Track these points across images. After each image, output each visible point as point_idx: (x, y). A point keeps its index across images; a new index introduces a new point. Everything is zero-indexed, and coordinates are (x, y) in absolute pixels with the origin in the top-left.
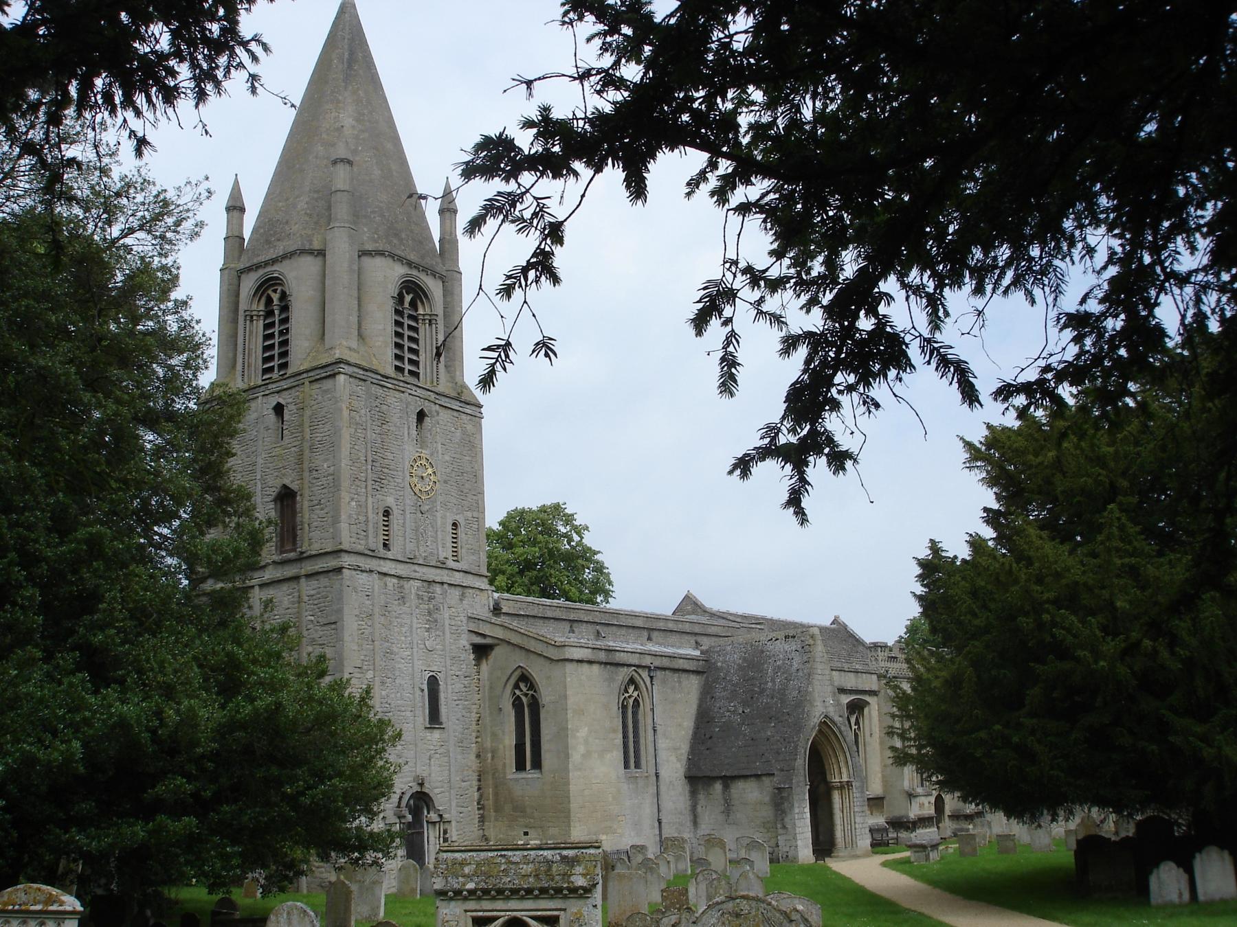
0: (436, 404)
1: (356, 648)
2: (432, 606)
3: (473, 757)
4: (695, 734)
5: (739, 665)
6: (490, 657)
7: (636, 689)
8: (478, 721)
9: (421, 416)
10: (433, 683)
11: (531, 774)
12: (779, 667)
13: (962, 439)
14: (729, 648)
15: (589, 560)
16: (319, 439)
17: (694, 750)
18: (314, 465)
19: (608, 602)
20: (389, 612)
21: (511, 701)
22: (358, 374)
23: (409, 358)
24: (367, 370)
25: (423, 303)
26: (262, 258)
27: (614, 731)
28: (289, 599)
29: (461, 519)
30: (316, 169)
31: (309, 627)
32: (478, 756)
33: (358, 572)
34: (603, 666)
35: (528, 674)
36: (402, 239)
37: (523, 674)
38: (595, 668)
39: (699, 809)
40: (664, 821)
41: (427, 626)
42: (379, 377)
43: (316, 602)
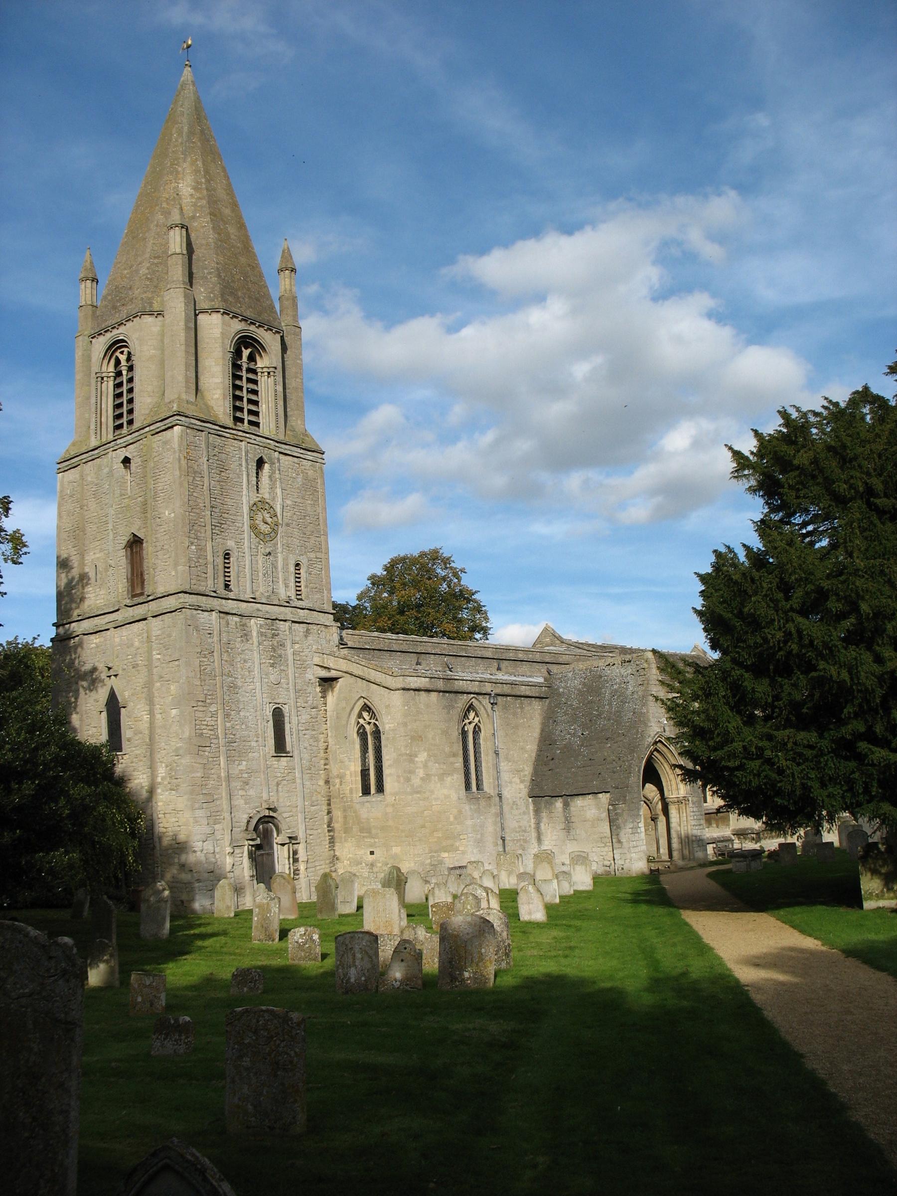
0: (275, 451)
1: (198, 683)
3: (321, 783)
4: (538, 756)
5: (579, 690)
6: (335, 689)
7: (477, 715)
8: (326, 749)
9: (260, 463)
10: (278, 717)
11: (374, 797)
12: (616, 691)
13: (730, 448)
14: (570, 675)
15: (468, 600)
16: (160, 488)
17: (536, 772)
18: (157, 513)
19: (487, 639)
20: (232, 649)
21: (356, 729)
22: (195, 424)
23: (248, 410)
24: (204, 422)
25: (261, 356)
26: (110, 322)
27: (455, 755)
30: (156, 236)
32: (327, 782)
33: (199, 612)
34: (441, 694)
36: (238, 298)
37: (365, 704)
38: (434, 695)
39: (542, 825)
40: (507, 838)
41: (271, 661)
42: (217, 428)
43: (162, 642)
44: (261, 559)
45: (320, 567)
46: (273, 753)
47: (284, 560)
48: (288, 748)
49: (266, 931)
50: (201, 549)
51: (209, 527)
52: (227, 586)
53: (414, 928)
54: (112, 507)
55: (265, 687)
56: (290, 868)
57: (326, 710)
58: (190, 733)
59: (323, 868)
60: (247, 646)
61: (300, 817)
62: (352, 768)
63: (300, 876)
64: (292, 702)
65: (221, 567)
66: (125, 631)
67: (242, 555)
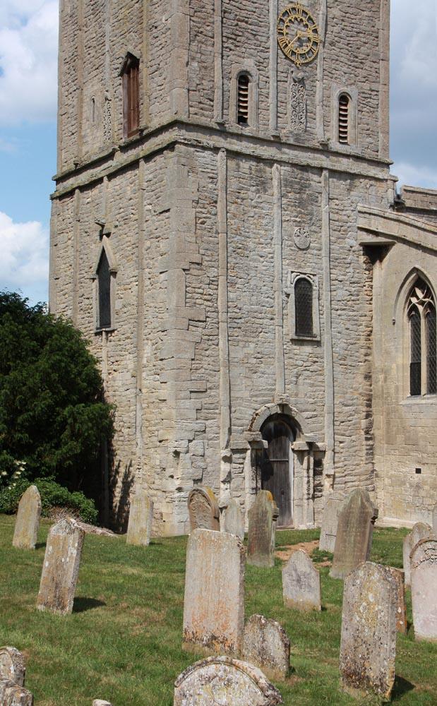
2: (305, 196)
8: (369, 335)
10: (303, 289)
21: (407, 311)
28: (131, 187)
29: (352, 91)
31: (148, 218)
35: (423, 278)
43: (153, 188)
44: (289, 85)
45: (376, 102)
46: (292, 335)
47: (325, 90)
48: (316, 330)
49: (56, 588)
50: (206, 68)
51: (218, 40)
52: (242, 120)
53: (262, 627)
54: (109, 21)
55: (287, 251)
56: (308, 482)
57: (372, 287)
58: (178, 301)
59: (359, 484)
60: (265, 197)
61: (327, 419)
62: (400, 361)
63: (323, 493)
64: (324, 273)
65: (233, 93)
66: (117, 180)
67: (265, 79)
